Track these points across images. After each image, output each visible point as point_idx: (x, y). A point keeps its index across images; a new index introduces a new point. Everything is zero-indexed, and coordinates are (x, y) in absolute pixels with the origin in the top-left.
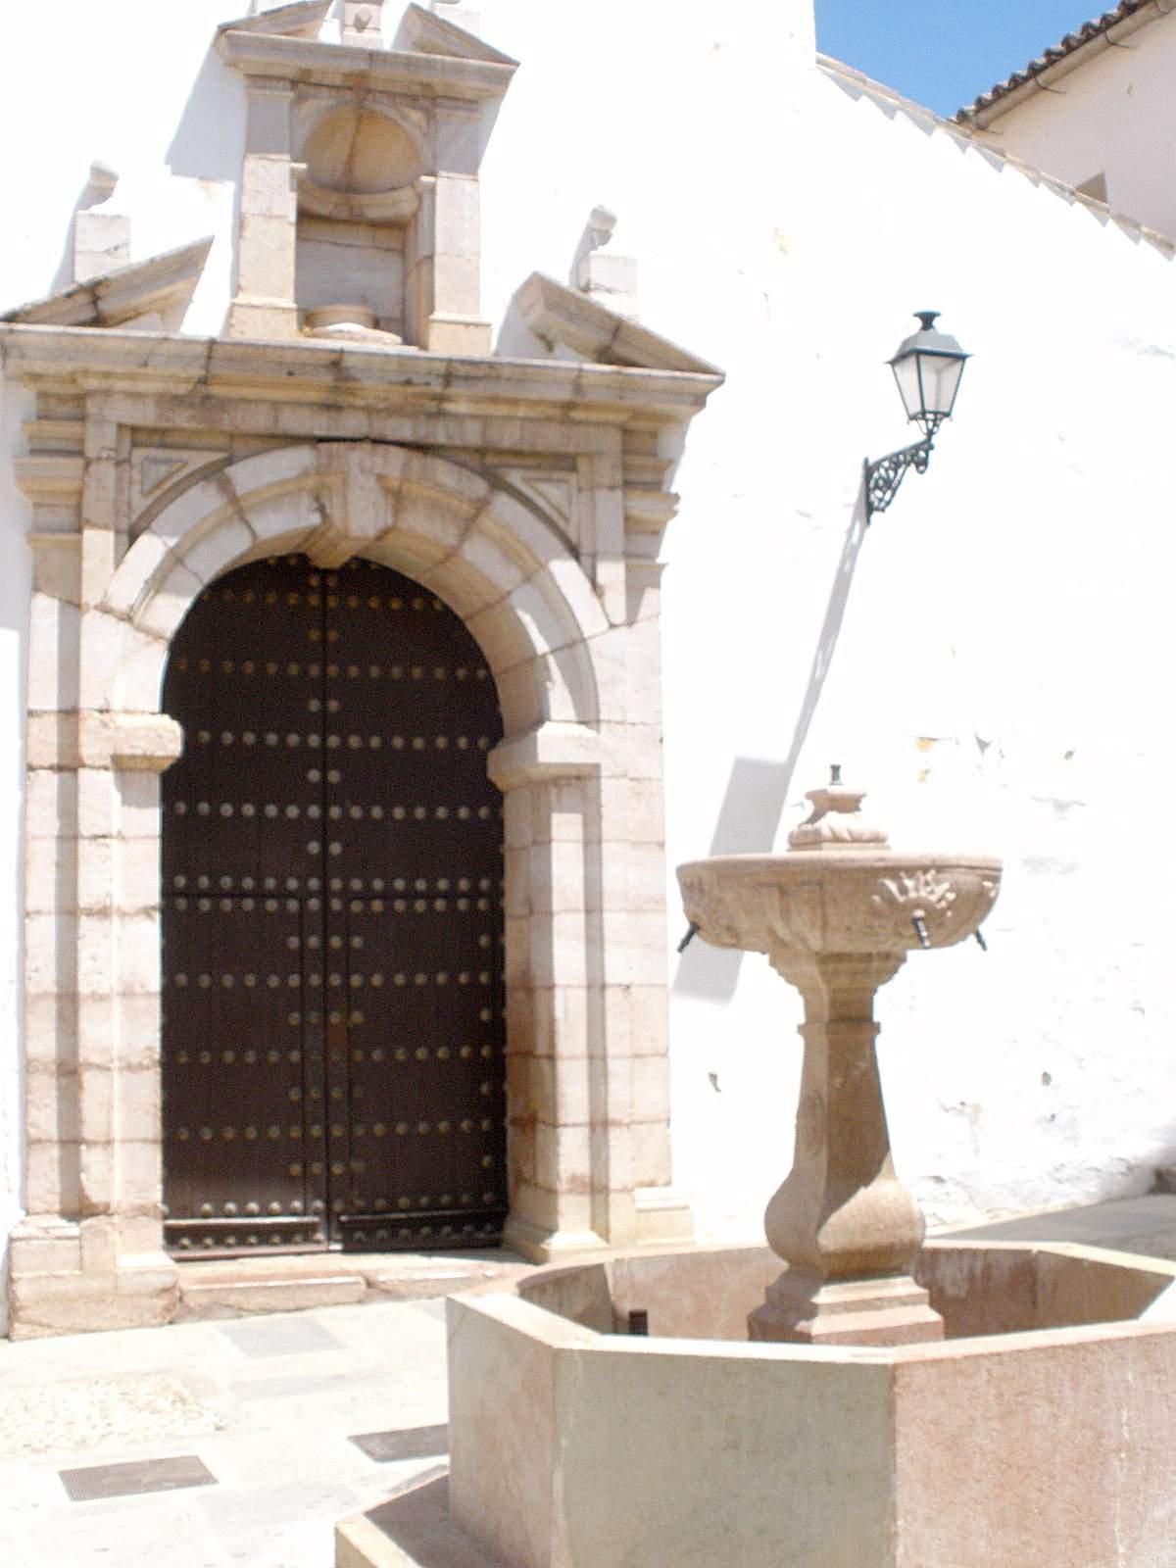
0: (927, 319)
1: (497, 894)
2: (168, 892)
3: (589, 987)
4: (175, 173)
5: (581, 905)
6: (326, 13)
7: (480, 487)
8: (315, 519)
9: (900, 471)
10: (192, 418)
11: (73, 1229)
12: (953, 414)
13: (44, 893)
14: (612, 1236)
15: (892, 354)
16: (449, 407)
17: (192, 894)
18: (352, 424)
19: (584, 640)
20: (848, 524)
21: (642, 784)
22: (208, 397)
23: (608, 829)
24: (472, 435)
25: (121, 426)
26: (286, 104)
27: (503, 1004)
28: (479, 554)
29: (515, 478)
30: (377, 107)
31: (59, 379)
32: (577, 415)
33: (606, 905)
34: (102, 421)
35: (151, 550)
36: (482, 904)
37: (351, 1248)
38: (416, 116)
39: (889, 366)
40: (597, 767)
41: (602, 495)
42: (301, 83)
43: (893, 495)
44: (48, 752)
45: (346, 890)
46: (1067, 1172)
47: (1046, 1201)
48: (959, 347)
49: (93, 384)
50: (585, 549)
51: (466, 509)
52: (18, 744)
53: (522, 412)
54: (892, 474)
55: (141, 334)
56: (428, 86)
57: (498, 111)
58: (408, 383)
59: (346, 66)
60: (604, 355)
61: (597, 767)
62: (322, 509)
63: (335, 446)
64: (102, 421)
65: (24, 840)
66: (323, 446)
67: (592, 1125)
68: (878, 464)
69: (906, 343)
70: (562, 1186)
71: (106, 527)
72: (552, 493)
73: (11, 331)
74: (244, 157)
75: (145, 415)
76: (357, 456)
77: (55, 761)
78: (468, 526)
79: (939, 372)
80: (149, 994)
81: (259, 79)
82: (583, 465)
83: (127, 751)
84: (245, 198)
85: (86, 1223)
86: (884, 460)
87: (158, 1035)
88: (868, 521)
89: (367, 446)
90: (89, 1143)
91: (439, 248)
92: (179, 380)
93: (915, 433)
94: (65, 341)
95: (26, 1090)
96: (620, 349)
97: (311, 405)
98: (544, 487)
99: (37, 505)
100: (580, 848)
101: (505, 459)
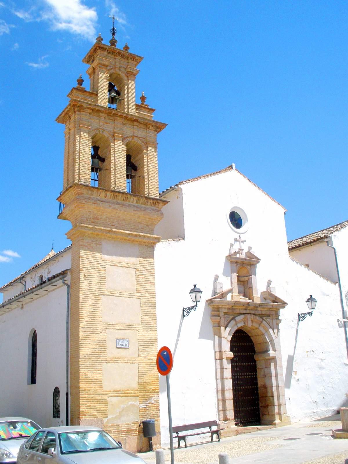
0: (195, 286)
1: (256, 375)
2: (232, 376)
3: (277, 387)
4: (224, 276)
5: (275, 376)
7: (261, 320)
8: (244, 324)
9: (190, 310)
10: (231, 311)
11: (226, 422)
12: (200, 301)
13: (219, 377)
14: (282, 420)
16: (258, 309)
17: (235, 376)
18: (248, 312)
19: (273, 340)
20: (297, 322)
21: (281, 359)
22: (233, 308)
23: (278, 365)
24: (260, 313)
25: (224, 312)
26: (235, 265)
27: (258, 390)
28: (261, 329)
29: (264, 318)
30: (244, 266)
31: (216, 306)
32: (271, 309)
33: (278, 375)
34: (222, 312)
35: (228, 329)
36: (254, 376)
37: (244, 426)
38: (249, 267)
40: (276, 357)
41: (274, 320)
42: (236, 262)
43: (189, 314)
44: (218, 357)
45: (239, 375)
46: (328, 411)
47: (326, 415)
49: (220, 307)
50: (272, 327)
51: (260, 322)
52: (214, 356)
53: (265, 309)
54: (189, 310)
55: (223, 300)
56: (250, 263)
58: (255, 306)
59: (241, 260)
60: (274, 301)
61: (276, 357)
62: (244, 323)
63: (246, 315)
64: (222, 312)
65: (216, 369)
66: (245, 315)
67: (278, 405)
68: (186, 309)
70: (276, 414)
71: (223, 326)
72: (269, 320)
73: (215, 300)
74: (231, 274)
75: (226, 311)
76: (249, 316)
77: (219, 358)
78: (260, 325)
80: (231, 389)
81: (232, 262)
82: (271, 316)
83: (228, 357)
84: (232, 280)
85: (227, 421)
86: (187, 308)
87: (232, 395)
88: (184, 318)
89: (249, 315)
90: (227, 410)
91: (253, 286)
93: (194, 304)
94: (221, 301)
95: (218, 403)
96: (276, 301)
97: (243, 309)
98: (267, 319)
99: (214, 323)
100: (274, 368)
101: (263, 316)
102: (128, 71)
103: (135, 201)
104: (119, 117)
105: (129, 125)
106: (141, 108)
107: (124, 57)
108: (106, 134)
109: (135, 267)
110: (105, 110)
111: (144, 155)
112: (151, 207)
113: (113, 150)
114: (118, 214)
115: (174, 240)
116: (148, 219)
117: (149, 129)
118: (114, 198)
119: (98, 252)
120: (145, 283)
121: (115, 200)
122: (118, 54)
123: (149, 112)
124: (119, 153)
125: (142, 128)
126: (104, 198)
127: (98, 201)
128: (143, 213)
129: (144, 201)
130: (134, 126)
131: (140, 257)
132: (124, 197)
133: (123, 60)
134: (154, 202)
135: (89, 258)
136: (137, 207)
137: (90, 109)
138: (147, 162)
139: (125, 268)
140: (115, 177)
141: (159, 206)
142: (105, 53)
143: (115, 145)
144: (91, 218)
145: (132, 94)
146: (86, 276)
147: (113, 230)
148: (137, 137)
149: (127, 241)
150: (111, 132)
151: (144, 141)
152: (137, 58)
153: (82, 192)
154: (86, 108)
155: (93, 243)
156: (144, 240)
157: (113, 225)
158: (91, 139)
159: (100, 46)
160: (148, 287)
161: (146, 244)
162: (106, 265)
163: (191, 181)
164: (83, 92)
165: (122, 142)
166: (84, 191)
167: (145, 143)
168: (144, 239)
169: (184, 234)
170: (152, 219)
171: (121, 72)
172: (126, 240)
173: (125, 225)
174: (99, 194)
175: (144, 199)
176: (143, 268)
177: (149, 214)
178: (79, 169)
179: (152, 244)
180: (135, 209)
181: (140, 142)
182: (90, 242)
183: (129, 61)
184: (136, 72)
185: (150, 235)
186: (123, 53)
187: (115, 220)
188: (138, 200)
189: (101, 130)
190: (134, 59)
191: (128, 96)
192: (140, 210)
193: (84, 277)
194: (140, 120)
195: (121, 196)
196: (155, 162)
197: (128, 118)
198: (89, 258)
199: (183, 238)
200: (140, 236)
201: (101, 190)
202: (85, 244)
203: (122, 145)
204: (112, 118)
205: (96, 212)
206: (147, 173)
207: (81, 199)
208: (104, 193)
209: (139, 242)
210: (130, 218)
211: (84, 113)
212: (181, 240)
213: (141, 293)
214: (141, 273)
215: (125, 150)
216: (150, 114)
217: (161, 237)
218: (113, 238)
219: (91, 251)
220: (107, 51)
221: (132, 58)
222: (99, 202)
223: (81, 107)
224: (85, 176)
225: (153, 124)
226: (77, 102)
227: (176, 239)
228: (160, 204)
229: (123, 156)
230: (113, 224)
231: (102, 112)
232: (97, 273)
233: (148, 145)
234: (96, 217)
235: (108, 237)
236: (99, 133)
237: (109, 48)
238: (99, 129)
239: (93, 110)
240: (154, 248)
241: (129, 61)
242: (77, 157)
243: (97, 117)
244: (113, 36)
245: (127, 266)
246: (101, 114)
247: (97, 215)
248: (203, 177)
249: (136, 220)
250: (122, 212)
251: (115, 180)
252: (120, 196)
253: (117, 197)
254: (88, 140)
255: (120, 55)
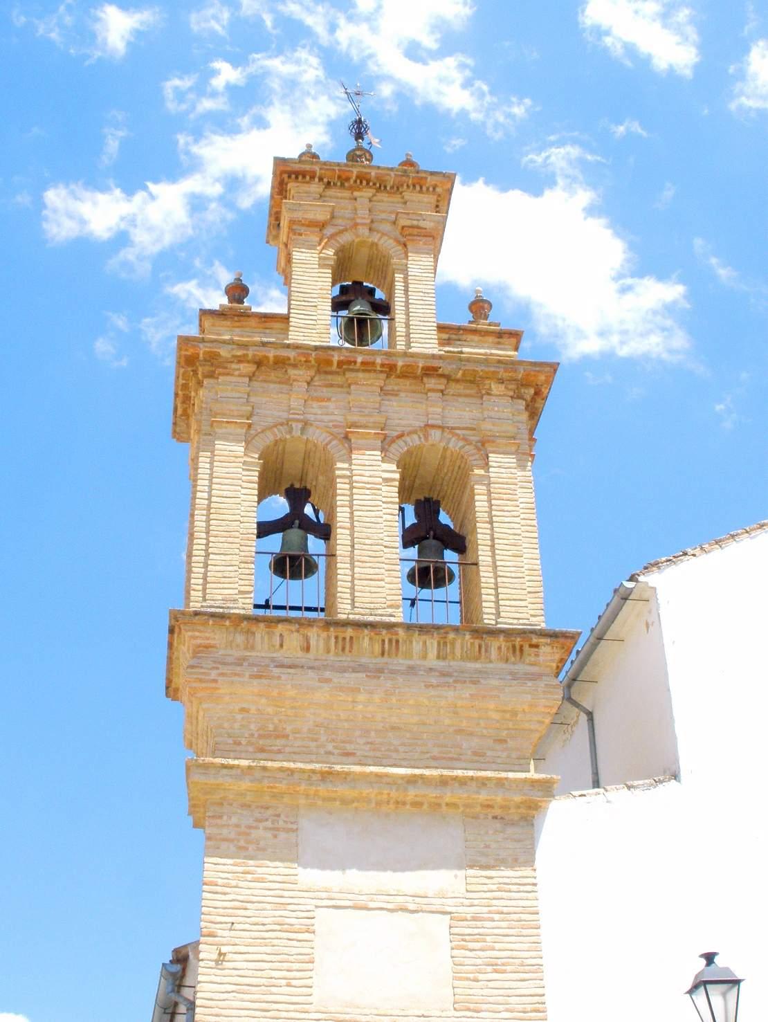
0: (710, 958)
6: (646, 357)
15: (689, 986)
39: (688, 995)
48: (735, 976)
57: (546, 814)
69: (697, 976)
79: (724, 995)
92: (365, 192)
102: (403, 227)
103: (433, 652)
104: (364, 371)
105: (409, 394)
106: (462, 334)
107: (385, 187)
108: (317, 436)
109: (449, 909)
110: (304, 354)
111: (476, 487)
112: (504, 666)
113: (347, 486)
114: (360, 707)
115: (629, 788)
116: (495, 716)
117: (488, 394)
118: (343, 649)
119: (282, 860)
120: (496, 971)
121: (349, 659)
122: (361, 182)
123: (499, 343)
124: (368, 492)
125: (460, 395)
126: (300, 654)
127: (276, 667)
128: (467, 691)
129: (472, 644)
130: (429, 394)
131: (471, 867)
132: (383, 641)
133: (383, 196)
134: (514, 647)
135: (241, 884)
136: (443, 674)
137: (249, 362)
138: (487, 509)
139: (400, 912)
140: (353, 576)
141: (541, 658)
142: (316, 187)
143: (353, 467)
144: (252, 735)
145: (421, 294)
146: (225, 954)
147: (338, 768)
148: (442, 428)
149: (408, 807)
150: (335, 426)
151: (472, 438)
152: (431, 180)
153: (208, 642)
154: (232, 362)
155: (261, 825)
156: (483, 796)
157: (348, 754)
158: (257, 461)
159: (289, 169)
160: (507, 984)
161: (498, 812)
162: (317, 907)
163: (694, 555)
164: (236, 318)
165: (379, 453)
166: (216, 636)
167: (479, 444)
168: (478, 793)
169: (676, 761)
170: (514, 713)
171: (379, 235)
172: (404, 803)
173: (401, 749)
174: (278, 643)
175: (468, 637)
176: (486, 909)
177: (495, 693)
178: (206, 565)
179: (523, 811)
180: (434, 681)
181: (454, 445)
182: (251, 822)
183: (407, 195)
184: (432, 224)
185: (503, 775)
186: (376, 174)
187: (358, 733)
188: (445, 643)
189: (294, 426)
190: (421, 188)
191: (407, 304)
192: (456, 681)
193: (217, 961)
194: (446, 368)
195: (371, 639)
196: (522, 506)
197: (399, 369)
198: (241, 884)
199: (675, 776)
200: (463, 782)
201: (280, 626)
202: (225, 831)
203: (380, 463)
204: (339, 379)
205: (270, 710)
206: (488, 548)
207: (202, 667)
208: (295, 634)
209: (462, 809)
210: (415, 719)
211: (228, 378)
212: (661, 782)
213: (478, 1011)
214: (476, 931)
215: (394, 480)
216: (501, 349)
217: (554, 776)
218: (345, 802)
219: (252, 858)
220: (321, 179)
221: (414, 186)
222: (277, 671)
223: (212, 358)
224: (226, 586)
225: (502, 374)
226: (194, 346)
227: (641, 782)
228: (543, 649)
229: (384, 500)
230: (350, 748)
231: (295, 366)
232: (275, 942)
233: (490, 449)
234: (276, 729)
235: (324, 799)
236: (288, 437)
237: (321, 169)
238: (288, 424)
239: (259, 363)
240: (533, 825)
241: (406, 197)
242: (200, 524)
243: (282, 386)
244: (358, 143)
245: (412, 907)
246: (292, 372)
247: (276, 721)
248: (747, 532)
249: (447, 722)
250: (377, 698)
251: (353, 588)
252: (367, 640)
253: (355, 647)
254: (245, 463)
255: (368, 184)
